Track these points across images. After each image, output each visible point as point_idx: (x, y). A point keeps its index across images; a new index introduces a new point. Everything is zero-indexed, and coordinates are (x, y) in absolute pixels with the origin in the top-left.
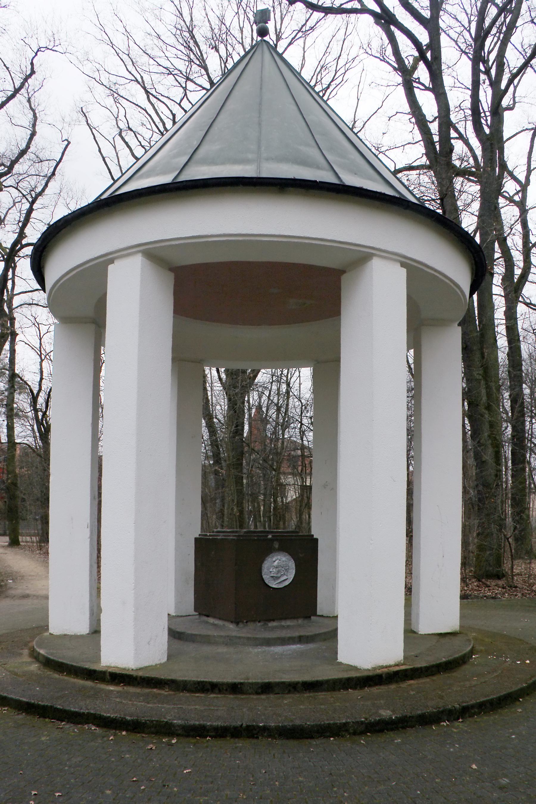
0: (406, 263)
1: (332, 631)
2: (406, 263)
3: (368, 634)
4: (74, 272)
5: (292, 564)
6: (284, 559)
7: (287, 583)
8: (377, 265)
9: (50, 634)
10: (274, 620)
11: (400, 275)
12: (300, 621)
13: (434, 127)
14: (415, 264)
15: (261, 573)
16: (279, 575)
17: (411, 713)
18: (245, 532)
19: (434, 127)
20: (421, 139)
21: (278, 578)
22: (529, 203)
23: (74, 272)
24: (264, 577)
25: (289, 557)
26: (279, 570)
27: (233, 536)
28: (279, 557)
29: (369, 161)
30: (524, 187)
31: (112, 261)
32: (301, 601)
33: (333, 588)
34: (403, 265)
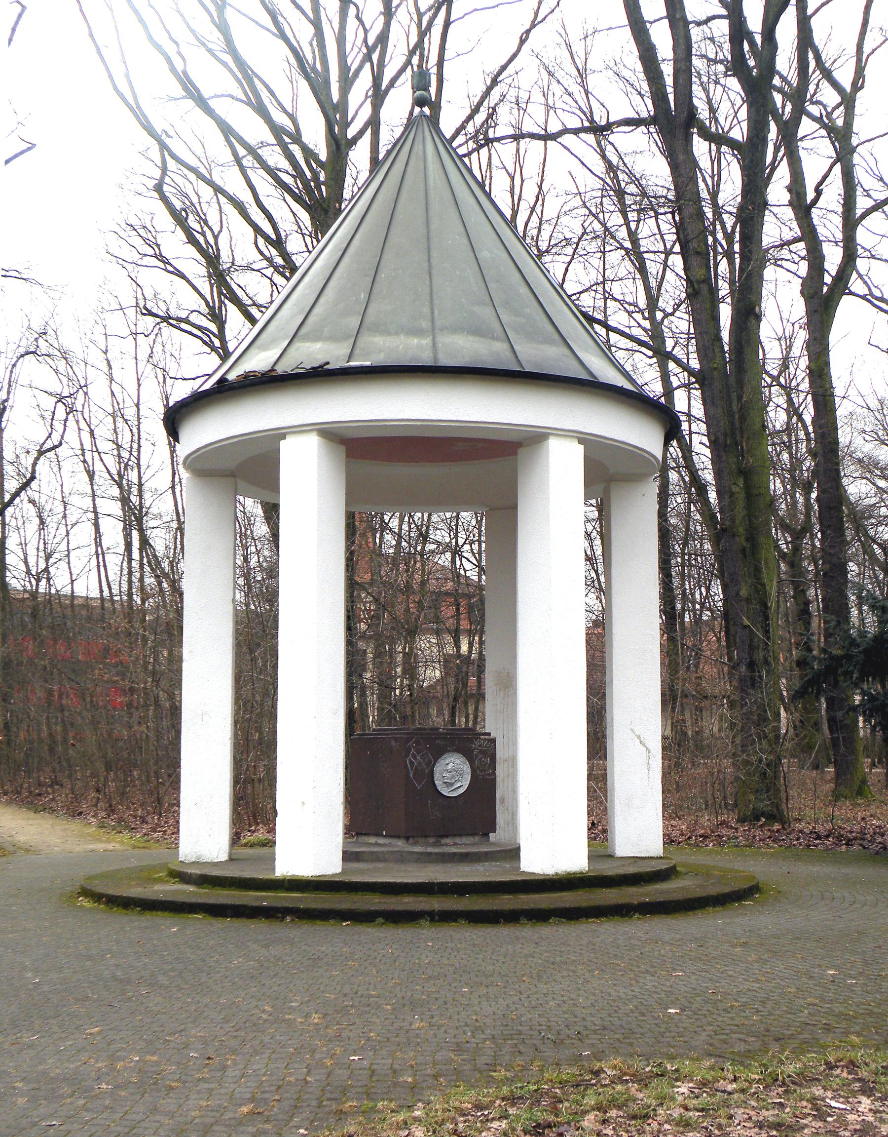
0: (584, 439)
1: (514, 849)
2: (584, 439)
3: (548, 837)
4: (236, 440)
5: (467, 769)
6: (458, 762)
7: (461, 791)
8: (553, 443)
9: (181, 862)
10: (447, 837)
11: (578, 451)
12: (477, 839)
13: (667, 70)
14: (594, 438)
15: (433, 777)
16: (453, 781)
17: (661, 1081)
18: (415, 729)
19: (667, 70)
20: (665, 14)
21: (452, 784)
22: (862, 128)
23: (236, 440)
24: (436, 782)
25: (463, 759)
26: (453, 774)
27: (404, 734)
28: (452, 759)
29: (544, 303)
30: (848, 101)
31: (283, 437)
32: (481, 808)
33: (513, 775)
34: (581, 441)
